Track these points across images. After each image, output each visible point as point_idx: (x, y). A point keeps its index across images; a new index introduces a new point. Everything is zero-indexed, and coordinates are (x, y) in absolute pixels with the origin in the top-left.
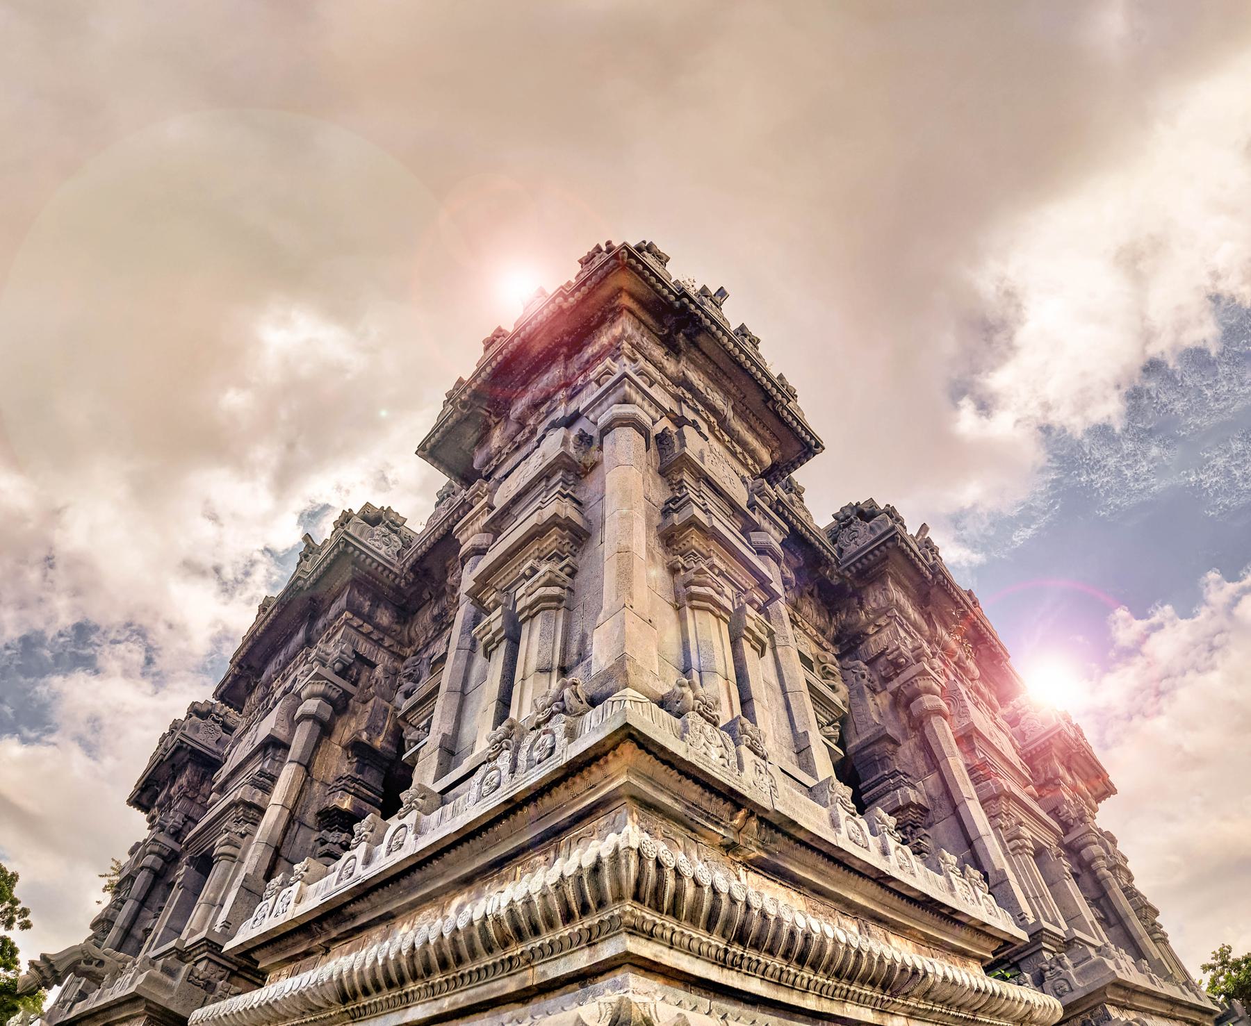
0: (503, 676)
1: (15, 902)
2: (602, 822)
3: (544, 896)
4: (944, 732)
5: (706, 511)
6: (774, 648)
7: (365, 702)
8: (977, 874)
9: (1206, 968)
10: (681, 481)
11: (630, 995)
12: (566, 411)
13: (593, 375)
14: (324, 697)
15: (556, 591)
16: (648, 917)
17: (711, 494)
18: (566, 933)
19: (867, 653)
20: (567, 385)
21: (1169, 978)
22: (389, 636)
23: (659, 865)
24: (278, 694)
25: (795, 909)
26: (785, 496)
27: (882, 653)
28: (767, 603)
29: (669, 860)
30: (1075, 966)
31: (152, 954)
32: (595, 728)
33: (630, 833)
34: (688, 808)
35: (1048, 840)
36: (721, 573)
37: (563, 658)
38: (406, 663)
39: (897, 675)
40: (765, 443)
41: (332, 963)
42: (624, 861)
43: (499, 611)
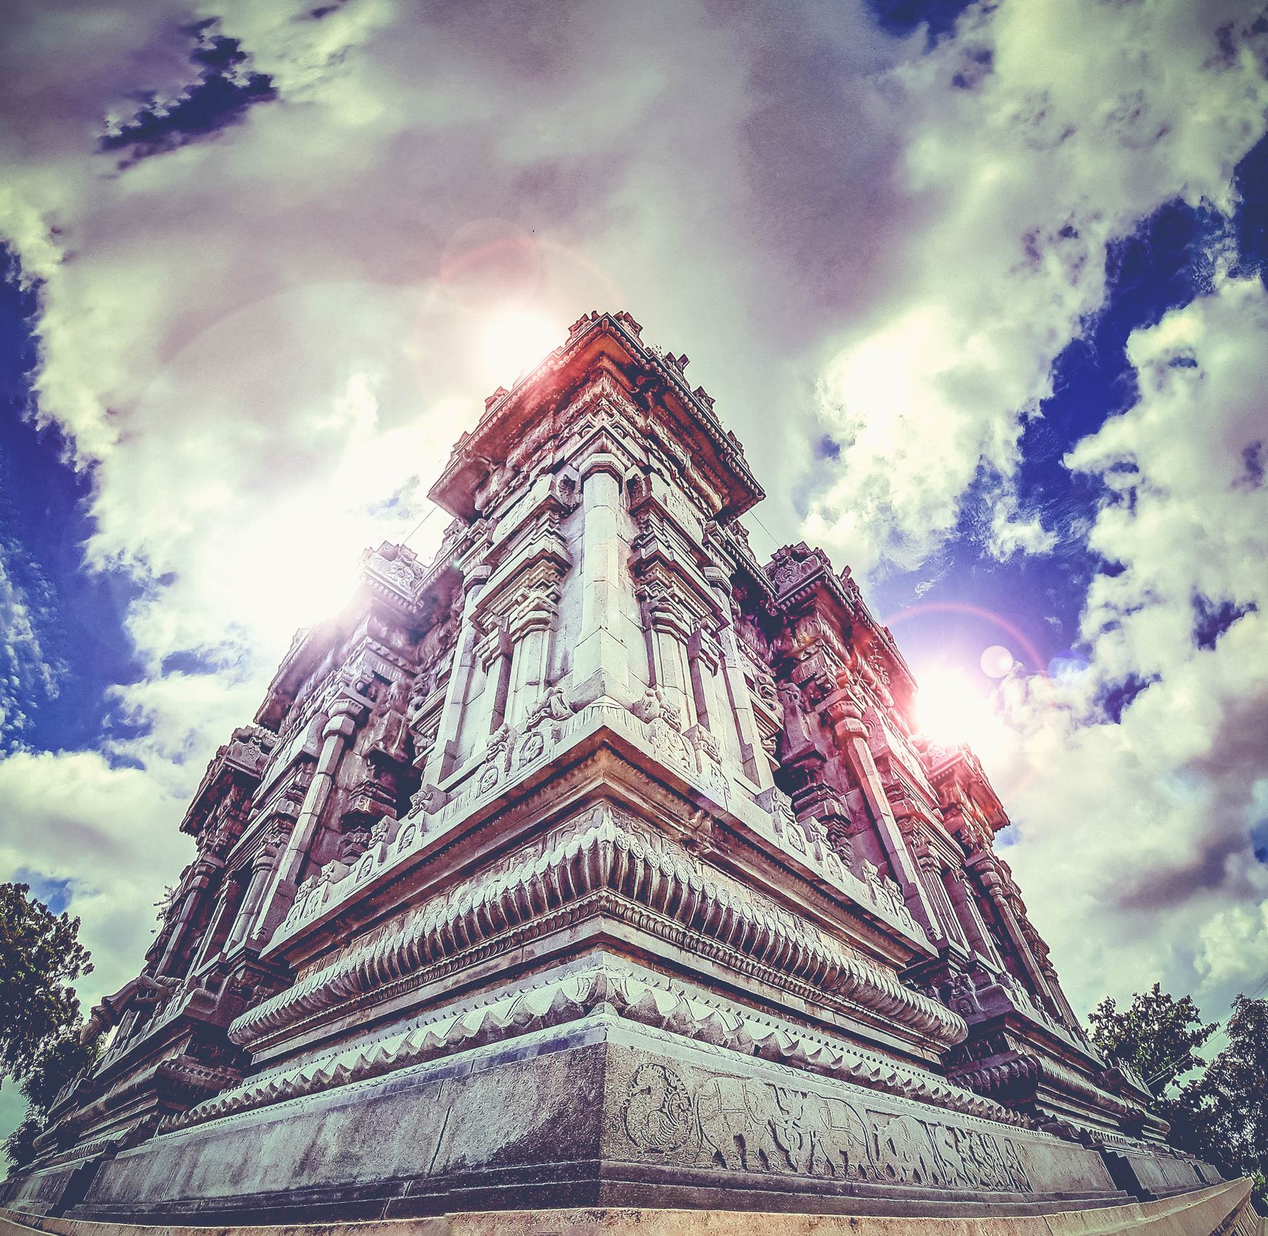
1: (80, 948)
2: (582, 818)
3: (533, 884)
4: (864, 752)
5: (669, 547)
6: (724, 669)
7: (382, 715)
8: (894, 885)
9: (1093, 1018)
14: (348, 713)
15: (544, 614)
16: (620, 902)
19: (798, 676)
20: (555, 437)
21: (1059, 1020)
23: (631, 857)
24: (308, 714)
26: (733, 538)
27: (812, 678)
28: (718, 629)
29: (637, 851)
30: (977, 988)
31: (197, 974)
32: (576, 731)
35: (954, 862)
36: (680, 602)
37: (548, 674)
39: (824, 698)
41: (355, 955)
42: (602, 852)
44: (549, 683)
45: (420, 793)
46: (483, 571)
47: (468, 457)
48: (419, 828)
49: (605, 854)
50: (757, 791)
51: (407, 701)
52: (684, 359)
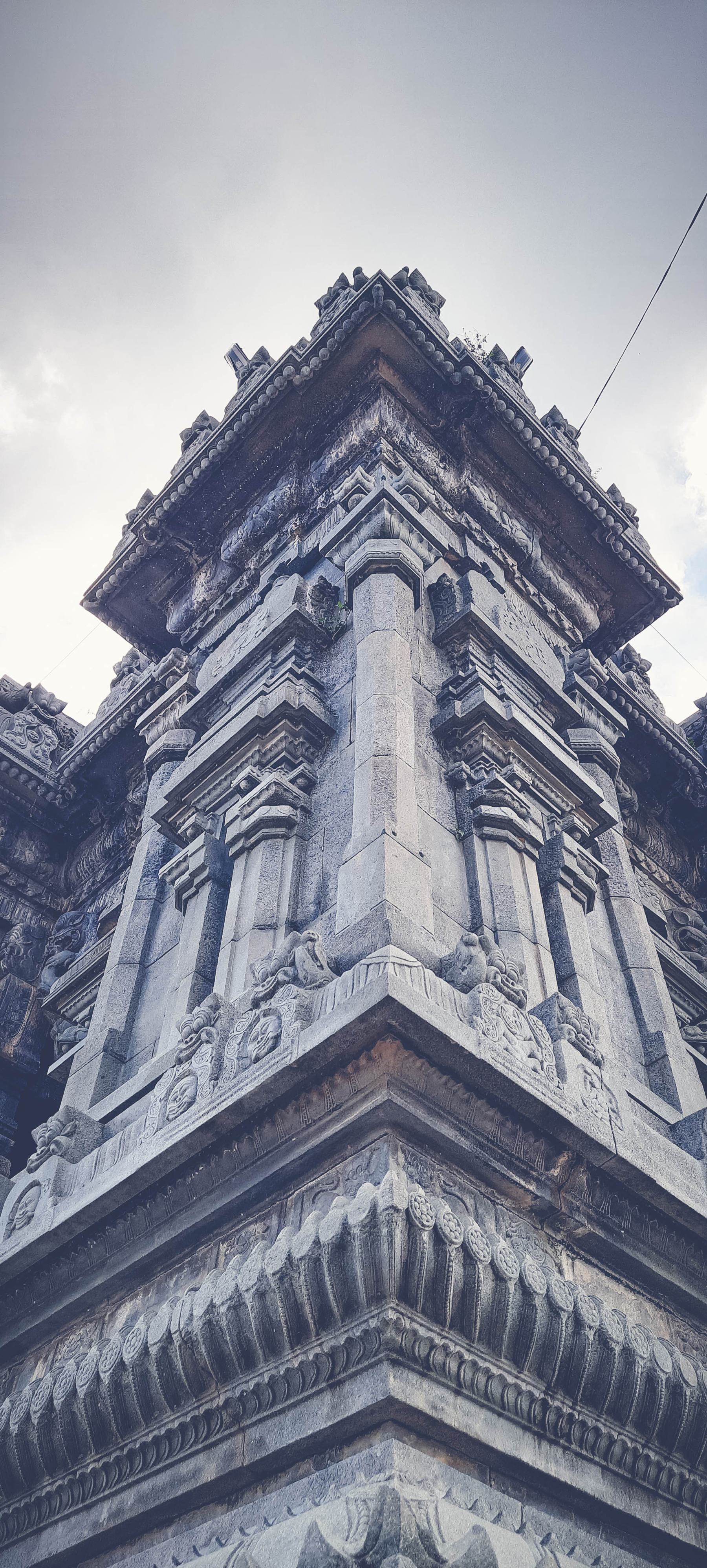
0: (205, 936)
2: (350, 1165)
3: (261, 1295)
5: (503, 697)
6: (607, 901)
10: (467, 652)
11: (395, 1483)
12: (300, 548)
13: (337, 494)
15: (284, 810)
16: (422, 1332)
17: (509, 672)
18: (296, 1363)
22: (35, 880)
25: (653, 1335)
26: (622, 676)
28: (595, 832)
32: (339, 1009)
33: (390, 1185)
34: (480, 1145)
36: (525, 788)
37: (294, 910)
38: (61, 920)
40: (589, 596)
42: (385, 1231)
43: (200, 840)
44: (294, 925)
45: (52, 1122)
46: (177, 738)
47: (151, 537)
48: (47, 1189)
49: (391, 1234)
50: (673, 1117)
51: (39, 959)
52: (521, 356)
